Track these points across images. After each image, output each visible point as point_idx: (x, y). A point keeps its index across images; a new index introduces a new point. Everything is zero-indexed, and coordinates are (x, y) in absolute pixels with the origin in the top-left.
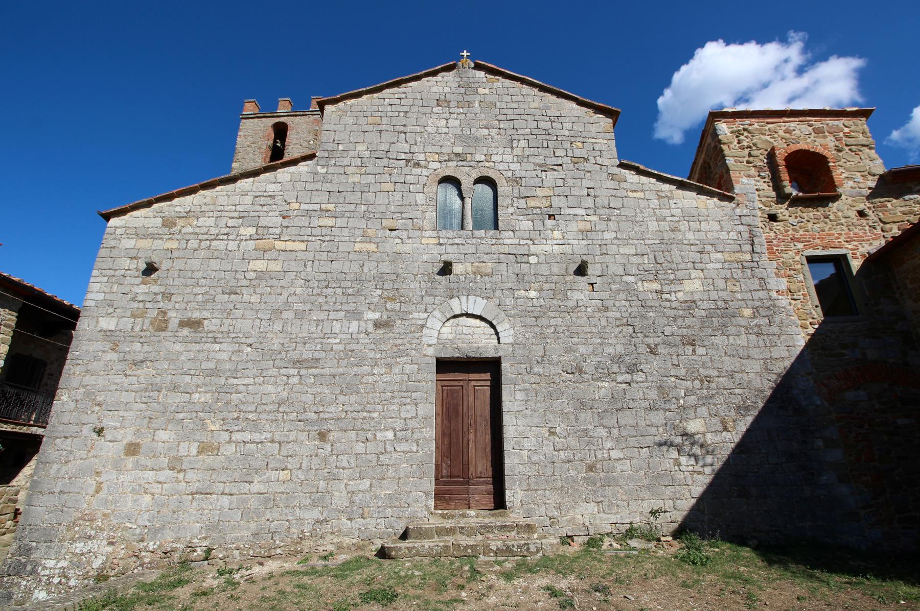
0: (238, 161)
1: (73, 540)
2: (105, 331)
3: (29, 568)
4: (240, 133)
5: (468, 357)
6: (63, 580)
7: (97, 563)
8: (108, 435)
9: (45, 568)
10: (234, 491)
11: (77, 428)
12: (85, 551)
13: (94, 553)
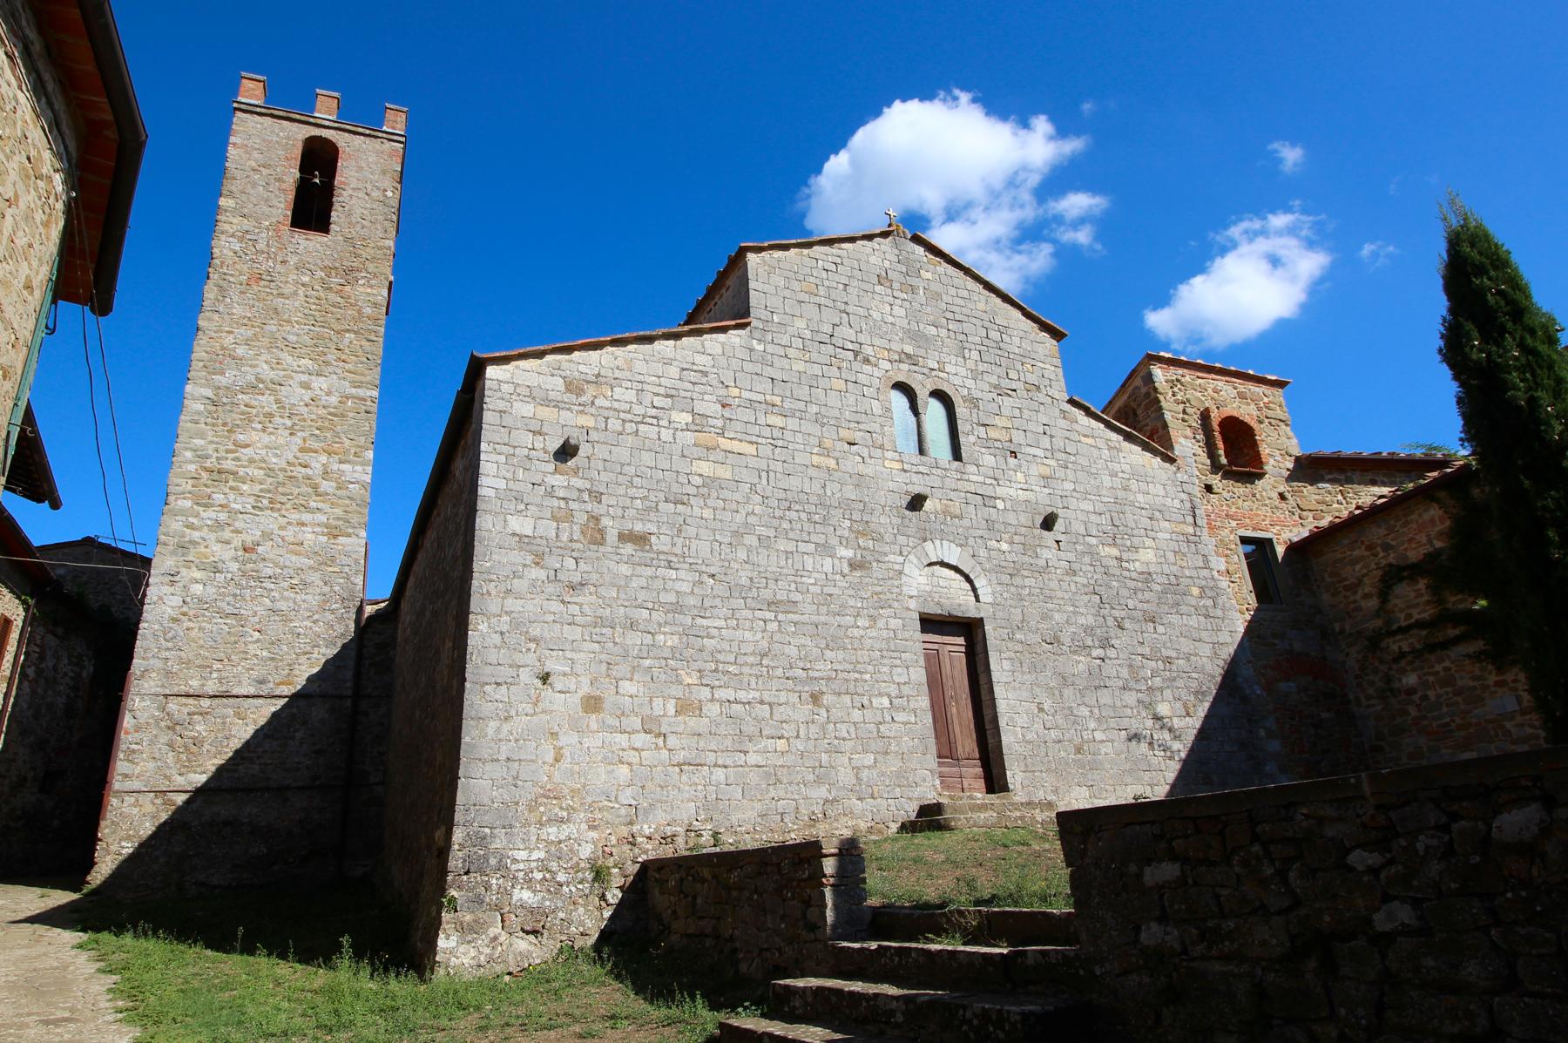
0: (231, 195)
2: (520, 536)
3: (493, 861)
4: (232, 139)
7: (586, 851)
9: (515, 861)
10: (729, 762)
12: (563, 837)
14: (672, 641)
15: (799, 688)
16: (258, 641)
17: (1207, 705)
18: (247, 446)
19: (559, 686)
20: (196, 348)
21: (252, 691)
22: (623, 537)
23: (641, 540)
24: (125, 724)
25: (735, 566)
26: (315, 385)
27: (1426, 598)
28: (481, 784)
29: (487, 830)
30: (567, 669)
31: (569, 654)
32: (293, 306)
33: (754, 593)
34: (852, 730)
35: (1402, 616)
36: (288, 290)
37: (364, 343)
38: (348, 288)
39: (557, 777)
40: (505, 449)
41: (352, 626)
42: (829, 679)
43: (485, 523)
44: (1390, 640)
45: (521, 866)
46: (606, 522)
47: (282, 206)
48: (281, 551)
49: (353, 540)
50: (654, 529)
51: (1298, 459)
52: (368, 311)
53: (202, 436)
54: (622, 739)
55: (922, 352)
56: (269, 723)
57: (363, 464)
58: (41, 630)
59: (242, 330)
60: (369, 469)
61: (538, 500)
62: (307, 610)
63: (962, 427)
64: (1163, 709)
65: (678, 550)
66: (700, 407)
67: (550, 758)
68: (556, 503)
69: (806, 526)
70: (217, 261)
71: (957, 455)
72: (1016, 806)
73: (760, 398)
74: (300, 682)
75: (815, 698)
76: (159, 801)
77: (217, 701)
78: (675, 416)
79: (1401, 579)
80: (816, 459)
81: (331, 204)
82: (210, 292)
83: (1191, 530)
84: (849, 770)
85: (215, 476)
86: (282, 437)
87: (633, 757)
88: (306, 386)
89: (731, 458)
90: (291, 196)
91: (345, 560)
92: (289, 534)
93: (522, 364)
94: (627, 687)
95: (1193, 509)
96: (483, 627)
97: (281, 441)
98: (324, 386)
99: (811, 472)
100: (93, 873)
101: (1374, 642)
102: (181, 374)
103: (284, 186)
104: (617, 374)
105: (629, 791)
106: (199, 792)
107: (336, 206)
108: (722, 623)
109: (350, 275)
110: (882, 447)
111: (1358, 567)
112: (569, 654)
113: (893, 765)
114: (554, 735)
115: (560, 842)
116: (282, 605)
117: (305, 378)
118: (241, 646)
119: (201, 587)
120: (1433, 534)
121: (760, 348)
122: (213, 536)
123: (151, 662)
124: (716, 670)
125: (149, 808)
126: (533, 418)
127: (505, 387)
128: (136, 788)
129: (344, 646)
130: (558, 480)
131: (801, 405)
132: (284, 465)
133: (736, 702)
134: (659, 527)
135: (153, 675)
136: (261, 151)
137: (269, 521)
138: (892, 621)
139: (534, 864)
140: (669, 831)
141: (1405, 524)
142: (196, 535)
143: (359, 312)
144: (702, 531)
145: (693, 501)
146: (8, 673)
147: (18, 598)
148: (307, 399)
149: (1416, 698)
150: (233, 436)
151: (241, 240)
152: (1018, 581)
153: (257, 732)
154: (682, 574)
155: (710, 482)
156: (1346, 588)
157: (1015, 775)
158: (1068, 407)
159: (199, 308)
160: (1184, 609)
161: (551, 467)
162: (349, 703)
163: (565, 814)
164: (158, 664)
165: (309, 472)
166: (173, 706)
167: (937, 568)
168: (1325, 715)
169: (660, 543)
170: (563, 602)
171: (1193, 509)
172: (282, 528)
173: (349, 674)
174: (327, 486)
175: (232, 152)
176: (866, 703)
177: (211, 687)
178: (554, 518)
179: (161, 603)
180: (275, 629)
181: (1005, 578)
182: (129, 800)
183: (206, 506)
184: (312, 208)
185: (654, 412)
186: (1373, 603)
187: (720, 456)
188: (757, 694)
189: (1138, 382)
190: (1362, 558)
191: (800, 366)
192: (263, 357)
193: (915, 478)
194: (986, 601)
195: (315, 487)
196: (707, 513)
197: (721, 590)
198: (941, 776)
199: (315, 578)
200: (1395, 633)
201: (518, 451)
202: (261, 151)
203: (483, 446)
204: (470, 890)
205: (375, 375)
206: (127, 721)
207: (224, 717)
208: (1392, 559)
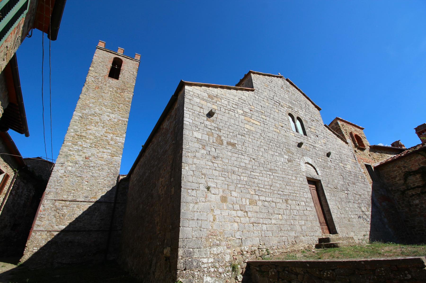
0: (93, 67)
1: (211, 247)
2: (198, 139)
3: (195, 264)
4: (95, 54)
5: (313, 178)
6: (215, 269)
7: (228, 258)
8: (213, 190)
9: (203, 263)
10: (267, 223)
11: (197, 185)
12: (219, 252)
13: (223, 253)
14: (246, 179)
15: (282, 198)
16: (87, 185)
17: (371, 208)
18: (90, 130)
19: (213, 192)
20: (78, 103)
21: (83, 200)
22: (229, 144)
23: (233, 145)
24: (40, 209)
25: (260, 157)
26: (111, 116)
27: (419, 180)
28: (189, 230)
29: (191, 250)
30: (215, 186)
31: (215, 181)
32: (107, 96)
33: (265, 166)
34: (297, 212)
35: (412, 185)
36: (106, 92)
37: (125, 107)
38: (122, 93)
39: (215, 227)
40: (192, 111)
41: (116, 182)
42: (289, 195)
43: (186, 132)
44: (409, 191)
45: (205, 265)
46: (223, 138)
47: (107, 72)
49: (118, 158)
50: (236, 142)
51: (370, 147)
52: (127, 99)
53: (77, 126)
54: (234, 213)
55: (293, 107)
56: (87, 210)
57: (122, 138)
58: (19, 180)
59: (92, 100)
60: (124, 139)
61: (202, 128)
62: (103, 176)
63: (305, 127)
64: (363, 209)
67: (212, 219)
68: (208, 130)
69: (275, 147)
70: (87, 82)
71: (305, 134)
72: (340, 239)
73: (259, 110)
74: (98, 198)
75: (287, 201)
76: (48, 234)
77: (71, 202)
78: (239, 111)
79: (411, 175)
80: (275, 129)
81: (120, 73)
82: (84, 89)
83: (355, 161)
84: (299, 226)
85: (79, 137)
86: (100, 128)
87: (237, 219)
88: (109, 116)
89: (254, 125)
90: (109, 70)
92: (99, 155)
93: (195, 87)
94: (234, 194)
95: (354, 156)
96: (187, 168)
97: (100, 129)
98: (114, 117)
99: (274, 133)
100: (22, 258)
101: (403, 192)
102: (73, 108)
104: (222, 96)
105: (238, 233)
106: (63, 231)
107: (121, 74)
109: (123, 90)
110: (289, 129)
111: (395, 173)
112: (215, 181)
113: (309, 224)
114: (212, 210)
115: (218, 254)
116: (95, 175)
117: (108, 114)
118: (81, 186)
119: (71, 168)
120: (420, 163)
121: (257, 97)
122: (76, 154)
123: (52, 189)
124: (259, 190)
125: (45, 236)
126: (199, 103)
127: (191, 93)
128: (41, 229)
129: (113, 188)
130: (208, 123)
132: (100, 136)
133: (266, 201)
134: (238, 142)
135: (52, 193)
136: (102, 59)
137: (94, 151)
138: (301, 178)
139: (210, 265)
140: (253, 248)
141: (410, 161)
142: (71, 153)
143: (125, 99)
144: (249, 145)
145: (246, 136)
146: (6, 192)
147: (13, 169)
148: (108, 119)
149: (419, 207)
150: (86, 127)
151: (94, 78)
152: (325, 170)
153: (83, 212)
154: (246, 157)
155: (249, 131)
156: (392, 178)
157: (338, 229)
158: (325, 127)
159: (81, 93)
161: (205, 119)
162: (113, 204)
163: (218, 242)
164: (54, 190)
165: (107, 138)
166: (57, 203)
168: (393, 212)
169: (239, 147)
170: (212, 162)
171: (354, 156)
172: (97, 153)
173: (114, 196)
174: (112, 142)
175: (94, 57)
176: (299, 204)
177: (70, 198)
178: (207, 134)
179: (57, 172)
180: (92, 182)
182: (38, 233)
183: (75, 145)
184: (115, 72)
186: (402, 182)
188: (271, 199)
189: (333, 125)
190: (397, 170)
191: (267, 104)
192: (97, 107)
193: (298, 139)
195: (109, 143)
196: (250, 140)
197: (257, 164)
199: (106, 167)
200: (410, 189)
201: (195, 112)
202: (102, 59)
203: (185, 108)
204: (187, 278)
205: (128, 115)
206: (41, 208)
207: (73, 208)
208: (406, 170)
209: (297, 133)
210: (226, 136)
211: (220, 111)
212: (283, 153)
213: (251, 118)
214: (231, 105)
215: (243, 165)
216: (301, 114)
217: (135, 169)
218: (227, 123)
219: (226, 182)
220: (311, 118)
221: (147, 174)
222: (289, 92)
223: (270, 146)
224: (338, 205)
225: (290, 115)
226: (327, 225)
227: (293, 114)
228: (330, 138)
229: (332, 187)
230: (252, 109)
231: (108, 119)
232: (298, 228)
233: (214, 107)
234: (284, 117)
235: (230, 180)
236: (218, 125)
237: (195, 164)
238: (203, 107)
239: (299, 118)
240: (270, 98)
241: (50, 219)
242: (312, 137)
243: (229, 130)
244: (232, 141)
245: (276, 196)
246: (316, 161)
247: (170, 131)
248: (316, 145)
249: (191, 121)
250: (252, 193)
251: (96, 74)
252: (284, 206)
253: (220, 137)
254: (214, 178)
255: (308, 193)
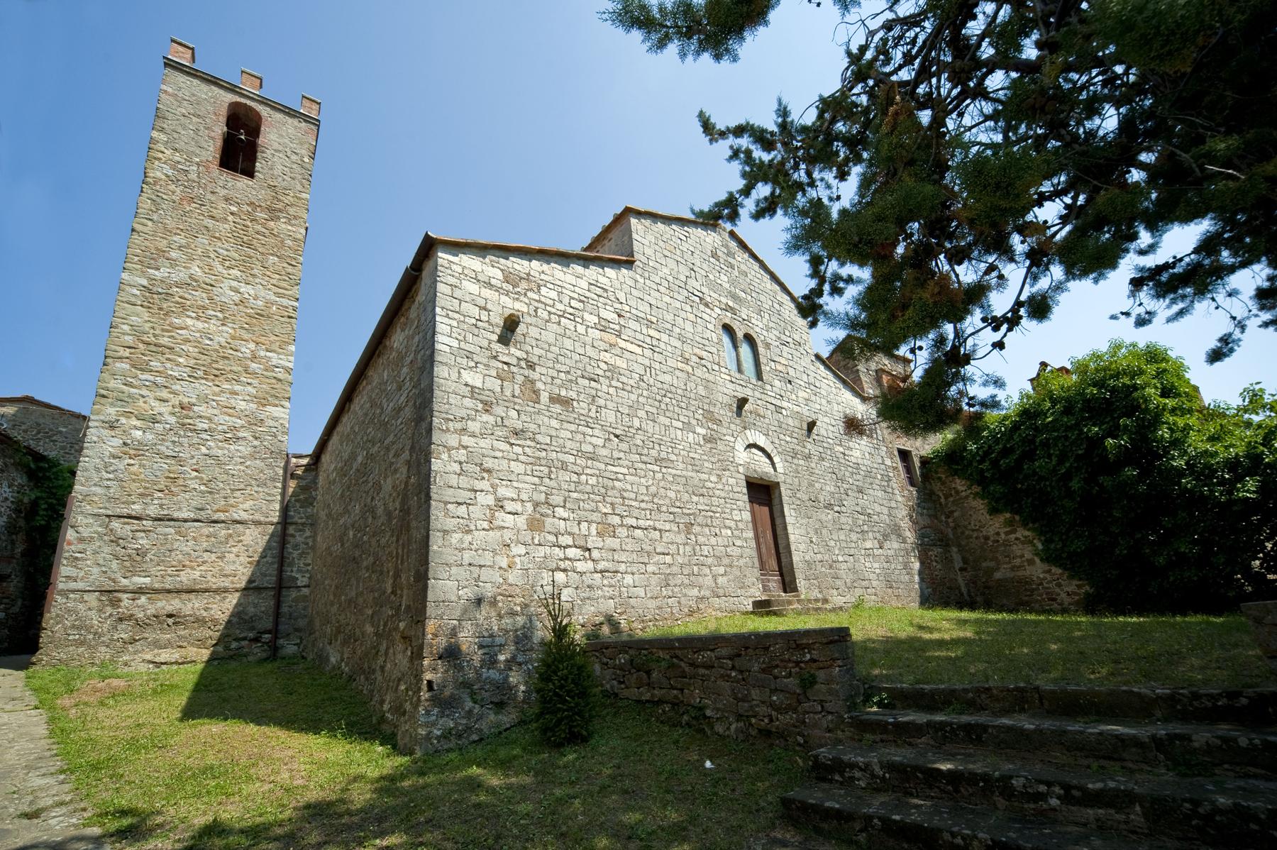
2: (472, 387)
14: (593, 481)
18: (182, 328)
22: (555, 399)
23: (566, 402)
31: (515, 484)
38: (272, 223)
43: (440, 371)
46: (539, 385)
47: (212, 149)
48: (215, 412)
50: (574, 396)
55: (737, 307)
61: (485, 361)
63: (763, 360)
65: (593, 414)
66: (604, 314)
68: (500, 365)
71: (759, 376)
73: (643, 315)
78: (586, 316)
80: (680, 365)
89: (627, 355)
90: (219, 143)
91: (271, 423)
92: (222, 398)
98: (252, 292)
103: (213, 134)
104: (543, 276)
108: (625, 471)
110: (718, 364)
112: (515, 484)
118: (181, 482)
121: (642, 280)
123: (93, 489)
131: (669, 326)
152: (795, 461)
157: (801, 583)
160: (875, 486)
166: (115, 524)
167: (754, 450)
169: (581, 407)
174: (254, 366)
177: (153, 511)
181: (789, 459)
185: (571, 310)
187: (618, 351)
191: (667, 299)
193: (739, 388)
194: (780, 471)
196: (612, 390)
198: (763, 581)
201: (467, 319)
203: (438, 310)
209: (738, 375)
210: (549, 380)
211: (536, 316)
212: (694, 422)
213: (619, 336)
214: (566, 300)
215: (587, 448)
216: (758, 328)
217: (331, 443)
218: (553, 348)
219: (543, 489)
220: (783, 337)
221: (360, 459)
222: (732, 267)
223: (663, 406)
224: (812, 534)
225: (727, 329)
226: (781, 575)
227: (736, 326)
228: (824, 386)
229: (805, 497)
230: (623, 313)
231: (237, 298)
232: (708, 581)
233: (518, 306)
234: (708, 334)
235: (553, 484)
236: (527, 353)
237: (465, 447)
238: (489, 306)
239: (749, 338)
240: (677, 282)
241: (101, 562)
242: (777, 383)
243: (558, 366)
244: (563, 393)
245: (665, 516)
246: (777, 441)
247: (408, 360)
248: (785, 404)
249: (455, 344)
250: (605, 510)
251: (177, 157)
252: (681, 539)
253: (533, 382)
254: (513, 477)
255: (741, 511)
